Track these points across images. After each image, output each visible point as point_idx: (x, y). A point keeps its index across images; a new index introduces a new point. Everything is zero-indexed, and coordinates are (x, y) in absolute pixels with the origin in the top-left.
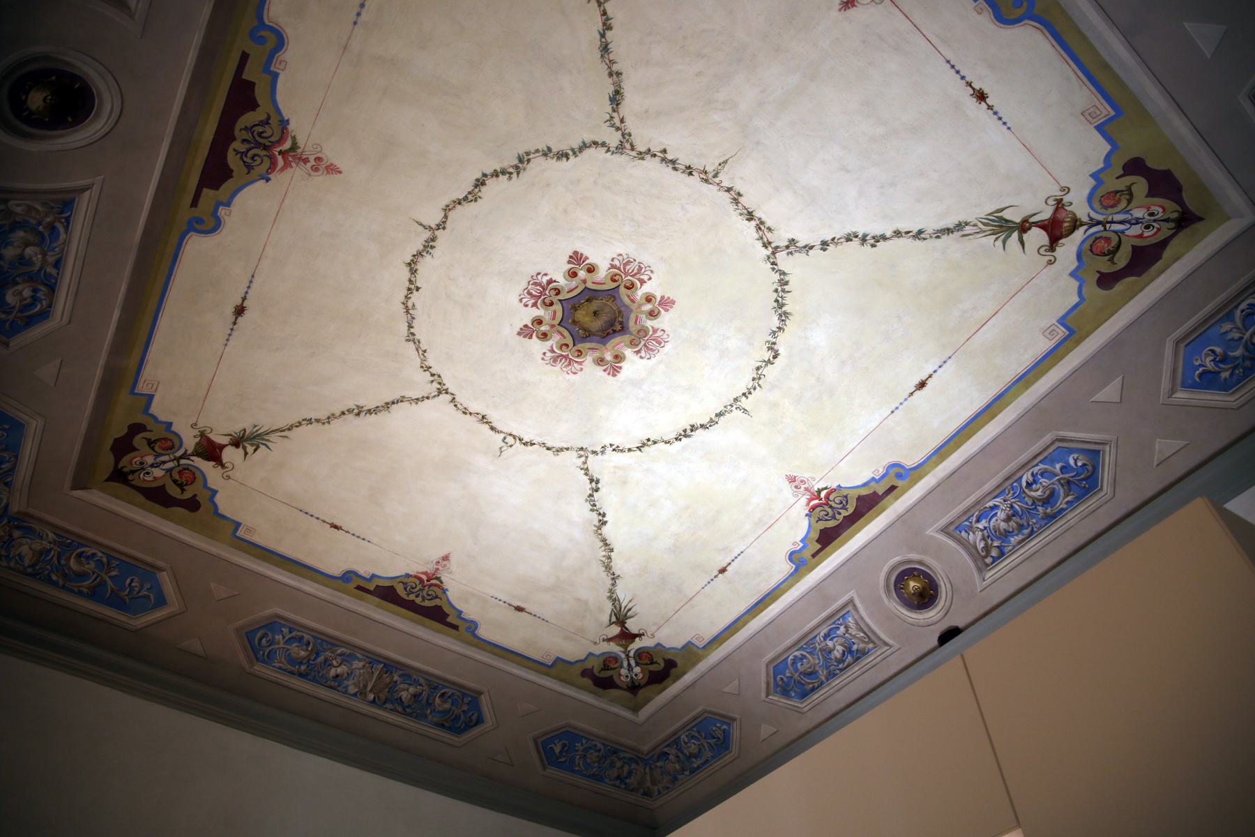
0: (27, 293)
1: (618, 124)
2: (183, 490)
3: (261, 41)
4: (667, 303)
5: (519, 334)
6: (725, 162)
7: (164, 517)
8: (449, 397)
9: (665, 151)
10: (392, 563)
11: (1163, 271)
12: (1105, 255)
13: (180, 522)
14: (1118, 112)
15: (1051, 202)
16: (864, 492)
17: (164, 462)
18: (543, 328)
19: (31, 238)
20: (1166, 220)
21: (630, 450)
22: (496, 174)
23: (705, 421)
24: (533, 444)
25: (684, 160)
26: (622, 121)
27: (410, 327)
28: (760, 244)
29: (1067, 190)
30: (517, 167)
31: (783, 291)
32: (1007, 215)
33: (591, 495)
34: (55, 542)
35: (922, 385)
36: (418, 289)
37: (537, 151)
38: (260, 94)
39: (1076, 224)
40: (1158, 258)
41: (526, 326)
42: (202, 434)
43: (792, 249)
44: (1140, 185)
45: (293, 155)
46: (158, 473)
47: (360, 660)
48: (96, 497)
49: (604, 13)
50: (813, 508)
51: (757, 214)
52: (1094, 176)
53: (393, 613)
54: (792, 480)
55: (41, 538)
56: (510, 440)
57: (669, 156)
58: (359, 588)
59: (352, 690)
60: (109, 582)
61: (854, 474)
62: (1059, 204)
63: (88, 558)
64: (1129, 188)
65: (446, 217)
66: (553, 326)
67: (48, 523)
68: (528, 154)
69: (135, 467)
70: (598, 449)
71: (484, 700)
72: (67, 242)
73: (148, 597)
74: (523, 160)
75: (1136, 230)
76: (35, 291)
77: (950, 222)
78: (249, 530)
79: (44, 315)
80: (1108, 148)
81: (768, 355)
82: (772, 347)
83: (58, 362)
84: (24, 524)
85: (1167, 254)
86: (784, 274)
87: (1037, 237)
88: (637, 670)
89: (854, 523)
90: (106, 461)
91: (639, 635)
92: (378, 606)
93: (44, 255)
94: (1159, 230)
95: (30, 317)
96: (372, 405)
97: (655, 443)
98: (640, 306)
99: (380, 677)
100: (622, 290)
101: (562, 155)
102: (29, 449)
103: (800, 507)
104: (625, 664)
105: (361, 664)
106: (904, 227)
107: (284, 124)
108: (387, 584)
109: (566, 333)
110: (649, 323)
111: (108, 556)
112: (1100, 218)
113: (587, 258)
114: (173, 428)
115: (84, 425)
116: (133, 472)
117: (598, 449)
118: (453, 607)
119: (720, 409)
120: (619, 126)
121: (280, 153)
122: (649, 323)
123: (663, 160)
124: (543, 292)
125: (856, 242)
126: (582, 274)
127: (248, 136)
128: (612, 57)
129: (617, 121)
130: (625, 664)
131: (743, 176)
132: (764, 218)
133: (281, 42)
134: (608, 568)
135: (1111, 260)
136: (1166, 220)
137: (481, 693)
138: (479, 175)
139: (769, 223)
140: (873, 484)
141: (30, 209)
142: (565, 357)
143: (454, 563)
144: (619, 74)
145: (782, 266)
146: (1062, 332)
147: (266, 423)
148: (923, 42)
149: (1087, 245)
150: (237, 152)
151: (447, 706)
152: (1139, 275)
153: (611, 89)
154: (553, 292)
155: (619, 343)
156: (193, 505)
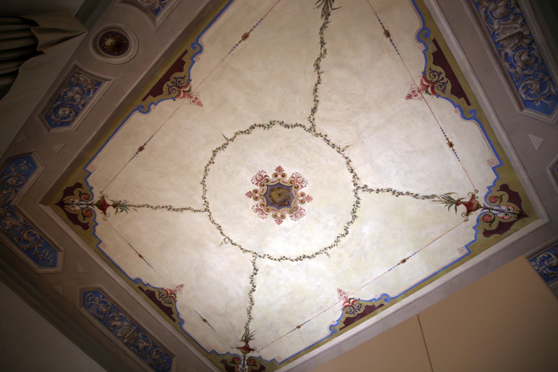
0: (67, 112)
1: (312, 120)
2: (84, 219)
3: (194, 48)
4: (309, 199)
5: (246, 194)
6: (348, 146)
7: (72, 228)
8: (209, 214)
9: (326, 136)
10: (158, 280)
11: (510, 235)
12: (488, 222)
13: (77, 233)
14: (501, 165)
15: (470, 195)
16: (369, 304)
17: (82, 204)
18: (257, 195)
19: (80, 91)
20: (514, 214)
21: (275, 259)
22: (260, 126)
23: (310, 255)
24: (236, 245)
25: (332, 141)
26: (314, 119)
27: (204, 178)
28: (353, 183)
29: (477, 191)
30: (268, 125)
31: (357, 206)
32: (452, 196)
33: (252, 276)
34: (22, 223)
35: (404, 261)
36: (213, 163)
37: (278, 122)
38: (185, 67)
39: (478, 207)
40: (509, 229)
41: (250, 192)
42: (103, 197)
43: (365, 189)
44: (506, 196)
45: (188, 94)
46: (77, 208)
47: (127, 322)
48: (48, 210)
49: (319, 77)
50: (346, 306)
51: (355, 171)
52: (488, 188)
53: (150, 304)
54: (340, 291)
55: (17, 220)
56: (227, 240)
57: (328, 138)
58: (140, 288)
59: (119, 334)
60: (36, 248)
61: (367, 295)
62: (473, 197)
63: (32, 235)
64: (501, 196)
65: (235, 137)
66: (261, 195)
67: (24, 215)
68: (274, 122)
69: (70, 202)
70: (262, 255)
71: (174, 359)
72: (91, 98)
73: (49, 261)
74: (272, 123)
75: (501, 215)
76: (71, 112)
77: (429, 194)
78: (104, 246)
79: (69, 124)
80: (495, 177)
81: (344, 232)
82: (346, 229)
83: (63, 145)
84: (13, 211)
85: (513, 227)
86: (359, 199)
87: (462, 208)
88: (247, 367)
89: (361, 318)
90: (60, 195)
91: (253, 350)
92: (145, 299)
93: (81, 100)
94: (510, 217)
95: (63, 122)
96: (176, 207)
97: (286, 259)
98: (298, 197)
99: (133, 333)
100: (293, 188)
101: (287, 126)
102: (33, 178)
103: (340, 305)
104: (242, 363)
105: (127, 324)
106: (411, 191)
107: (189, 80)
108: (152, 290)
109: (265, 200)
110: (300, 205)
111: (41, 238)
112: (488, 206)
113: (283, 170)
114: (92, 191)
115: (59, 176)
116: (68, 204)
117: (262, 255)
118: (177, 310)
119: (318, 251)
120: (312, 120)
121: (183, 91)
122: (300, 205)
123: (325, 139)
124: (261, 179)
125: (391, 193)
126: (279, 176)
127: (174, 81)
128: (317, 94)
129: (312, 119)
130: (242, 363)
131: (354, 154)
132: (357, 173)
133: (201, 50)
134: (249, 312)
135: (490, 225)
136: (514, 214)
137: (174, 356)
138: (253, 124)
139: (358, 176)
140: (374, 301)
141: (86, 80)
142: (261, 211)
143: (184, 290)
144: (318, 101)
145: (359, 195)
146: (466, 251)
147: (130, 201)
148: (433, 118)
149: (481, 217)
150: (168, 85)
151: (157, 357)
152: (500, 234)
153: (313, 106)
154: (266, 181)
155: (285, 211)
156: (85, 227)
